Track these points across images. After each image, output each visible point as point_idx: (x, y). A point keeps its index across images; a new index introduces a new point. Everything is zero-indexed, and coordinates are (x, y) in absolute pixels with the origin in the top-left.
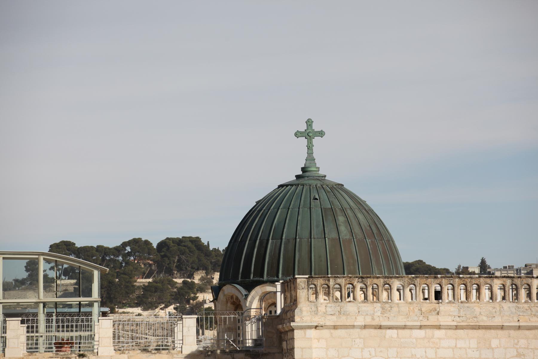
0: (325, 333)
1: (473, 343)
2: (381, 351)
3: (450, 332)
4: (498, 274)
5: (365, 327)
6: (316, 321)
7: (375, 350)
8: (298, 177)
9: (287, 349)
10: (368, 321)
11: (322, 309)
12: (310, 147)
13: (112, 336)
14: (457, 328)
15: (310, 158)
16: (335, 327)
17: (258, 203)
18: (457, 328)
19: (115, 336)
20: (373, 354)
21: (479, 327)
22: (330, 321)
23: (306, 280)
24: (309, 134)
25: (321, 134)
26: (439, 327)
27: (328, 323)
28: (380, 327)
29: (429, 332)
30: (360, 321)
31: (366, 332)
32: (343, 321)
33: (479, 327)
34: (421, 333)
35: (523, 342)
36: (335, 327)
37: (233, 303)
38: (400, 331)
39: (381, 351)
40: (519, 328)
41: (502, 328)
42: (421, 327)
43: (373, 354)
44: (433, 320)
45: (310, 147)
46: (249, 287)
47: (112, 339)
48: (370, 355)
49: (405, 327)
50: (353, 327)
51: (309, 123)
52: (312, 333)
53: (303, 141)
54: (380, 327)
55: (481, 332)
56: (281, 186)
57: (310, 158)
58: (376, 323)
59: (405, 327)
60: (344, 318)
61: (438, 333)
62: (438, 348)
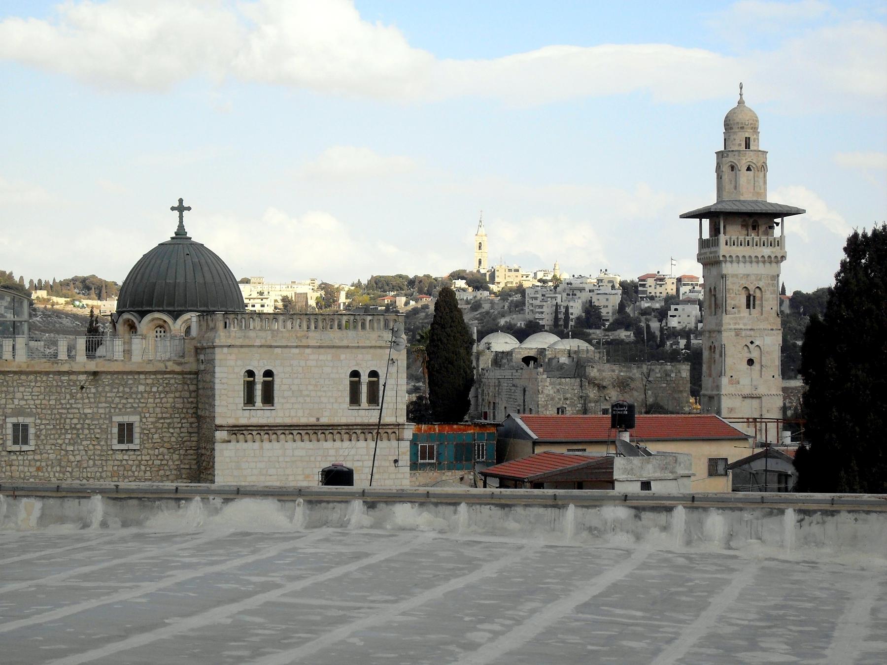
0: (235, 350)
1: (329, 357)
3: (315, 350)
4: (664, 324)
5: (261, 346)
6: (230, 342)
8: (172, 238)
10: (263, 342)
11: (233, 334)
12: (181, 217)
14: (320, 347)
15: (181, 226)
16: (242, 346)
18: (320, 347)
21: (333, 347)
22: (238, 342)
24: (181, 208)
25: (189, 209)
26: (308, 347)
27: (237, 344)
28: (271, 347)
29: (302, 350)
30: (258, 343)
31: (261, 349)
32: (247, 342)
33: (333, 347)
34: (296, 351)
35: (360, 356)
36: (242, 346)
37: (129, 325)
38: (284, 349)
40: (358, 347)
41: (348, 347)
42: (297, 347)
44: (304, 342)
45: (181, 217)
46: (142, 314)
49: (286, 347)
50: (254, 346)
51: (181, 201)
52: (225, 350)
53: (177, 213)
54: (271, 347)
55: (333, 350)
57: (181, 226)
58: (268, 343)
59: (286, 347)
60: (247, 340)
61: (308, 351)
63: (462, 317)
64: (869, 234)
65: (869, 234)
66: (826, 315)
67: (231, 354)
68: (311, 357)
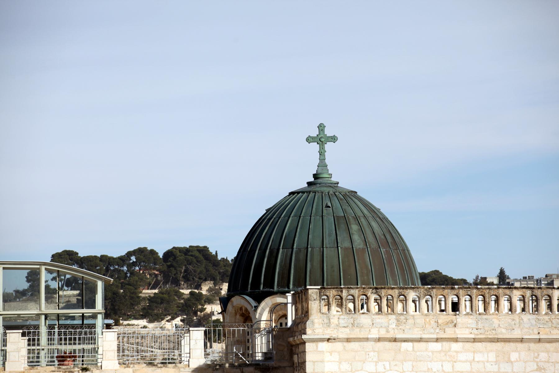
0: (338, 346)
1: (492, 357)
2: (396, 365)
3: (468, 345)
5: (379, 340)
7: (390, 364)
8: (309, 184)
9: (299, 363)
10: (383, 333)
11: (334, 321)
12: (322, 153)
13: (116, 349)
14: (475, 340)
15: (322, 164)
16: (348, 340)
17: (268, 210)
18: (475, 340)
19: (120, 349)
20: (388, 367)
21: (498, 340)
22: (343, 333)
23: (318, 291)
24: (321, 139)
25: (334, 139)
26: (456, 340)
27: (341, 336)
28: (395, 340)
30: (374, 334)
32: (356, 333)
33: (498, 340)
34: (437, 346)
35: (543, 356)
36: (348, 340)
38: (416, 344)
39: (396, 365)
40: (540, 340)
41: (522, 340)
42: (437, 340)
43: (388, 367)
44: (450, 332)
45: (322, 153)
47: (116, 352)
48: (385, 369)
49: (420, 340)
50: (367, 339)
51: (321, 127)
52: (324, 346)
53: (315, 147)
54: (395, 340)
55: (499, 345)
56: (292, 193)
57: (322, 164)
58: (390, 335)
59: (420, 340)
60: (357, 330)
61: (455, 346)
62: (455, 362)
63: (307, 321)
64: (219, 258)
65: (219, 258)
66: (265, 354)
67: (331, 353)
68: (462, 357)
